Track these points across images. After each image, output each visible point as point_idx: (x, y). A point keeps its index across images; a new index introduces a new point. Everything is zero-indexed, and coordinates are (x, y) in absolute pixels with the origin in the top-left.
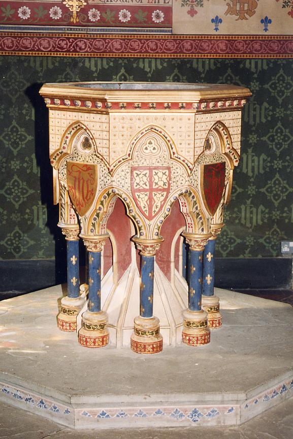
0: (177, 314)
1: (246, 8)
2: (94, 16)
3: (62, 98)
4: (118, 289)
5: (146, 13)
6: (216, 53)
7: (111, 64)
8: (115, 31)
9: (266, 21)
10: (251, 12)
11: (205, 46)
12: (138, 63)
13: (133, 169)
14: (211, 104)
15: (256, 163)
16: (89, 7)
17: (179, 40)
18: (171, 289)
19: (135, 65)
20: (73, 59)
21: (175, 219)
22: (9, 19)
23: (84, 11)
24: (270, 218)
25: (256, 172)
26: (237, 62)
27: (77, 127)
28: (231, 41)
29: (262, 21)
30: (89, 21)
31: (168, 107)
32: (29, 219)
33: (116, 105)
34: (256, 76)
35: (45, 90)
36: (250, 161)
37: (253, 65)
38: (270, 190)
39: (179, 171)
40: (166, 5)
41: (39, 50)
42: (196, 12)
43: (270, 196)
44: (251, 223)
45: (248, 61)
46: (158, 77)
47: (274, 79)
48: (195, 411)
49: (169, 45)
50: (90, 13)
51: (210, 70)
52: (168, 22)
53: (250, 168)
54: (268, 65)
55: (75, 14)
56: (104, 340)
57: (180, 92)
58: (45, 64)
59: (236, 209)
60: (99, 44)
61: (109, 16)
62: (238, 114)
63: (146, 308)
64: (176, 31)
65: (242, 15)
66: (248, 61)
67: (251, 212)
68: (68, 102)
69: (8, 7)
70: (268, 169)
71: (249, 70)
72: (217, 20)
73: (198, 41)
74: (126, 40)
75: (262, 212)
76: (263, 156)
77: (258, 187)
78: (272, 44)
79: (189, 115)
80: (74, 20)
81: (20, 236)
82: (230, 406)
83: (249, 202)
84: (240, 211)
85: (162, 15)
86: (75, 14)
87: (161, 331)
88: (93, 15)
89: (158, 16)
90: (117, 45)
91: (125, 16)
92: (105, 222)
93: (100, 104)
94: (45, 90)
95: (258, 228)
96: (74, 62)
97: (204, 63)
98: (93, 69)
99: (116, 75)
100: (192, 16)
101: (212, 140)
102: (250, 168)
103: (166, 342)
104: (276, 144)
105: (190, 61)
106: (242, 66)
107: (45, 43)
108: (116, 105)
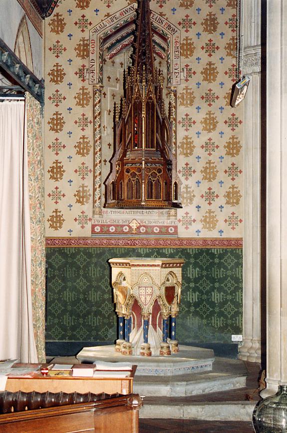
0: (158, 344)
1: (211, 226)
2: (143, 230)
3: (116, 264)
4: (135, 336)
5: (166, 229)
6: (198, 246)
7: (150, 251)
8: (153, 236)
9: (221, 232)
10: (214, 228)
11: (193, 243)
12: (162, 250)
13: (139, 287)
14: (167, 265)
15: (219, 296)
16: (141, 226)
17: (181, 240)
18: (156, 336)
19: (161, 251)
20: (133, 249)
21: (157, 308)
22: (105, 232)
23: (138, 228)
24: (226, 324)
25: (219, 301)
26: (208, 250)
27: (121, 274)
28: (205, 241)
29: (219, 232)
30: (140, 232)
31: (151, 266)
32: (112, 322)
33: (133, 265)
34: (217, 256)
35: (110, 261)
36: (216, 296)
37: (216, 251)
38: (226, 310)
39: (156, 288)
40: (175, 225)
41: (118, 245)
42: (188, 228)
43: (226, 313)
44: (217, 325)
45: (213, 250)
46: (148, 255)
47: (226, 258)
48: (156, 370)
49: (177, 242)
50: (141, 229)
51: (196, 254)
52: (176, 232)
53: (216, 299)
54: (223, 251)
55: (134, 229)
56: (130, 353)
57: (17, 231)
58: (121, 251)
59: (209, 319)
60: (145, 242)
61: (149, 230)
62: (181, 269)
63: (146, 341)
64: (179, 236)
65: (209, 229)
66: (213, 250)
67: (217, 320)
68: (125, 265)
69: (105, 227)
70: (224, 300)
71: (214, 254)
72: (198, 231)
73: (190, 240)
74: (157, 240)
75: (223, 320)
76: (222, 293)
77: (220, 308)
78: (144, 241)
79: (159, 268)
80: (134, 232)
81: (108, 330)
82: (169, 368)
83: (216, 315)
84: (211, 319)
85: (173, 229)
86: (134, 229)
87: (151, 349)
88: (142, 230)
89: (171, 230)
90: (153, 242)
91: (157, 230)
92: (131, 307)
93: (128, 265)
94: (110, 261)
95: (220, 328)
96: (134, 250)
97: (193, 250)
98: (142, 253)
99: (153, 255)
100: (187, 229)
101: (170, 278)
102: (216, 299)
103: (153, 353)
104: (228, 288)
105: (186, 249)
106: (210, 252)
107: (121, 242)
108: (133, 265)
